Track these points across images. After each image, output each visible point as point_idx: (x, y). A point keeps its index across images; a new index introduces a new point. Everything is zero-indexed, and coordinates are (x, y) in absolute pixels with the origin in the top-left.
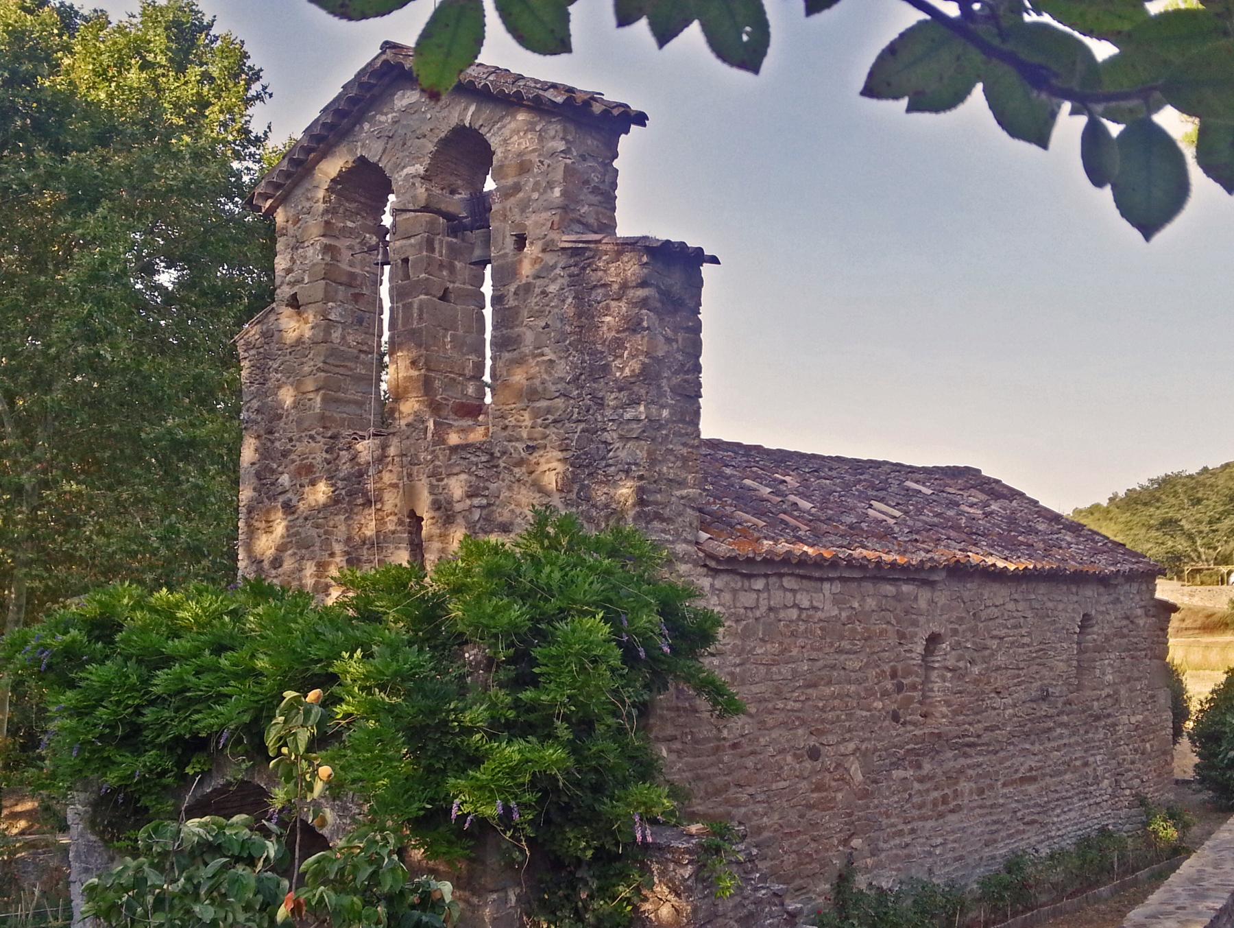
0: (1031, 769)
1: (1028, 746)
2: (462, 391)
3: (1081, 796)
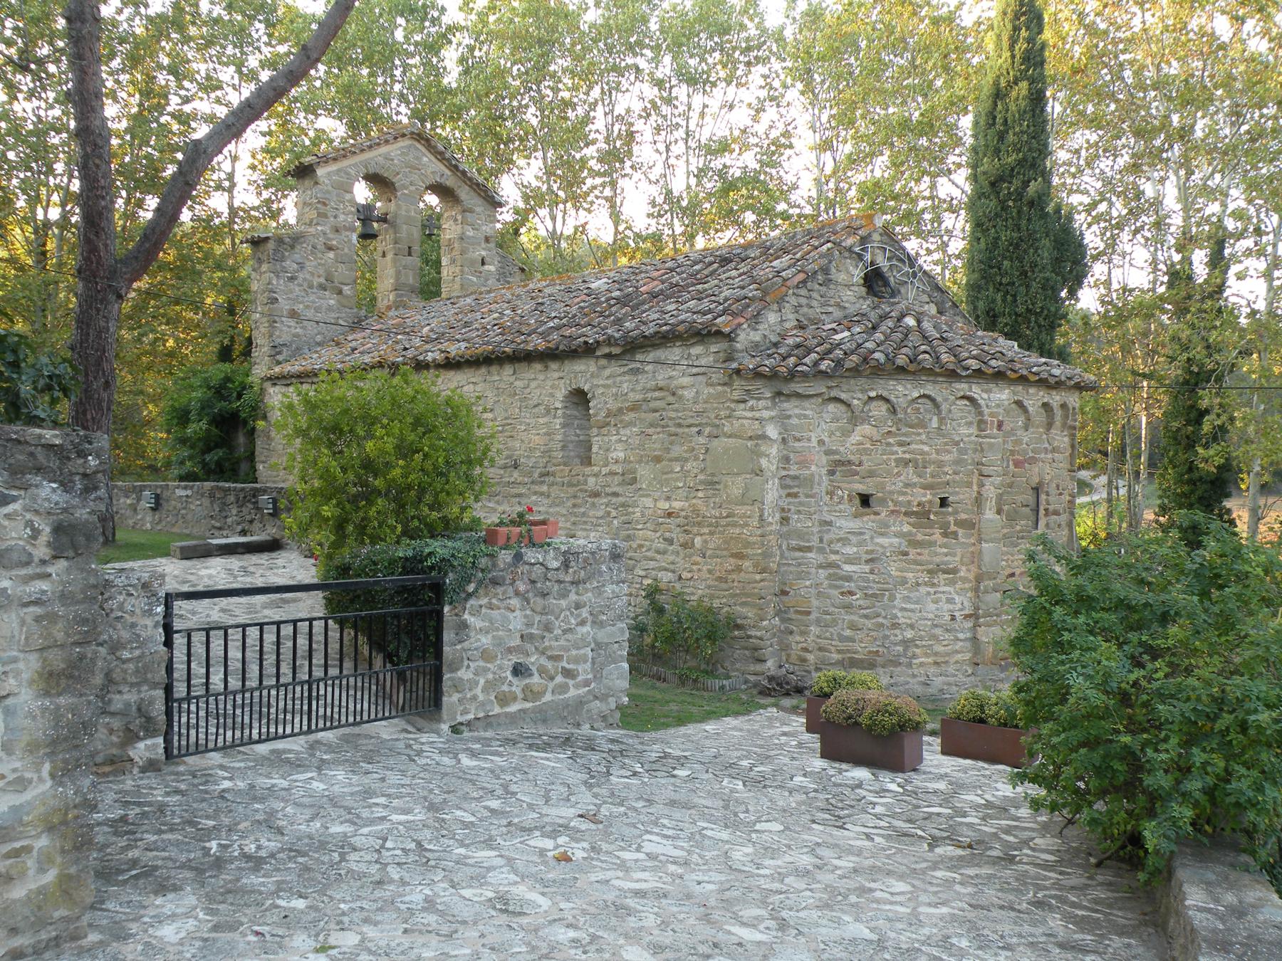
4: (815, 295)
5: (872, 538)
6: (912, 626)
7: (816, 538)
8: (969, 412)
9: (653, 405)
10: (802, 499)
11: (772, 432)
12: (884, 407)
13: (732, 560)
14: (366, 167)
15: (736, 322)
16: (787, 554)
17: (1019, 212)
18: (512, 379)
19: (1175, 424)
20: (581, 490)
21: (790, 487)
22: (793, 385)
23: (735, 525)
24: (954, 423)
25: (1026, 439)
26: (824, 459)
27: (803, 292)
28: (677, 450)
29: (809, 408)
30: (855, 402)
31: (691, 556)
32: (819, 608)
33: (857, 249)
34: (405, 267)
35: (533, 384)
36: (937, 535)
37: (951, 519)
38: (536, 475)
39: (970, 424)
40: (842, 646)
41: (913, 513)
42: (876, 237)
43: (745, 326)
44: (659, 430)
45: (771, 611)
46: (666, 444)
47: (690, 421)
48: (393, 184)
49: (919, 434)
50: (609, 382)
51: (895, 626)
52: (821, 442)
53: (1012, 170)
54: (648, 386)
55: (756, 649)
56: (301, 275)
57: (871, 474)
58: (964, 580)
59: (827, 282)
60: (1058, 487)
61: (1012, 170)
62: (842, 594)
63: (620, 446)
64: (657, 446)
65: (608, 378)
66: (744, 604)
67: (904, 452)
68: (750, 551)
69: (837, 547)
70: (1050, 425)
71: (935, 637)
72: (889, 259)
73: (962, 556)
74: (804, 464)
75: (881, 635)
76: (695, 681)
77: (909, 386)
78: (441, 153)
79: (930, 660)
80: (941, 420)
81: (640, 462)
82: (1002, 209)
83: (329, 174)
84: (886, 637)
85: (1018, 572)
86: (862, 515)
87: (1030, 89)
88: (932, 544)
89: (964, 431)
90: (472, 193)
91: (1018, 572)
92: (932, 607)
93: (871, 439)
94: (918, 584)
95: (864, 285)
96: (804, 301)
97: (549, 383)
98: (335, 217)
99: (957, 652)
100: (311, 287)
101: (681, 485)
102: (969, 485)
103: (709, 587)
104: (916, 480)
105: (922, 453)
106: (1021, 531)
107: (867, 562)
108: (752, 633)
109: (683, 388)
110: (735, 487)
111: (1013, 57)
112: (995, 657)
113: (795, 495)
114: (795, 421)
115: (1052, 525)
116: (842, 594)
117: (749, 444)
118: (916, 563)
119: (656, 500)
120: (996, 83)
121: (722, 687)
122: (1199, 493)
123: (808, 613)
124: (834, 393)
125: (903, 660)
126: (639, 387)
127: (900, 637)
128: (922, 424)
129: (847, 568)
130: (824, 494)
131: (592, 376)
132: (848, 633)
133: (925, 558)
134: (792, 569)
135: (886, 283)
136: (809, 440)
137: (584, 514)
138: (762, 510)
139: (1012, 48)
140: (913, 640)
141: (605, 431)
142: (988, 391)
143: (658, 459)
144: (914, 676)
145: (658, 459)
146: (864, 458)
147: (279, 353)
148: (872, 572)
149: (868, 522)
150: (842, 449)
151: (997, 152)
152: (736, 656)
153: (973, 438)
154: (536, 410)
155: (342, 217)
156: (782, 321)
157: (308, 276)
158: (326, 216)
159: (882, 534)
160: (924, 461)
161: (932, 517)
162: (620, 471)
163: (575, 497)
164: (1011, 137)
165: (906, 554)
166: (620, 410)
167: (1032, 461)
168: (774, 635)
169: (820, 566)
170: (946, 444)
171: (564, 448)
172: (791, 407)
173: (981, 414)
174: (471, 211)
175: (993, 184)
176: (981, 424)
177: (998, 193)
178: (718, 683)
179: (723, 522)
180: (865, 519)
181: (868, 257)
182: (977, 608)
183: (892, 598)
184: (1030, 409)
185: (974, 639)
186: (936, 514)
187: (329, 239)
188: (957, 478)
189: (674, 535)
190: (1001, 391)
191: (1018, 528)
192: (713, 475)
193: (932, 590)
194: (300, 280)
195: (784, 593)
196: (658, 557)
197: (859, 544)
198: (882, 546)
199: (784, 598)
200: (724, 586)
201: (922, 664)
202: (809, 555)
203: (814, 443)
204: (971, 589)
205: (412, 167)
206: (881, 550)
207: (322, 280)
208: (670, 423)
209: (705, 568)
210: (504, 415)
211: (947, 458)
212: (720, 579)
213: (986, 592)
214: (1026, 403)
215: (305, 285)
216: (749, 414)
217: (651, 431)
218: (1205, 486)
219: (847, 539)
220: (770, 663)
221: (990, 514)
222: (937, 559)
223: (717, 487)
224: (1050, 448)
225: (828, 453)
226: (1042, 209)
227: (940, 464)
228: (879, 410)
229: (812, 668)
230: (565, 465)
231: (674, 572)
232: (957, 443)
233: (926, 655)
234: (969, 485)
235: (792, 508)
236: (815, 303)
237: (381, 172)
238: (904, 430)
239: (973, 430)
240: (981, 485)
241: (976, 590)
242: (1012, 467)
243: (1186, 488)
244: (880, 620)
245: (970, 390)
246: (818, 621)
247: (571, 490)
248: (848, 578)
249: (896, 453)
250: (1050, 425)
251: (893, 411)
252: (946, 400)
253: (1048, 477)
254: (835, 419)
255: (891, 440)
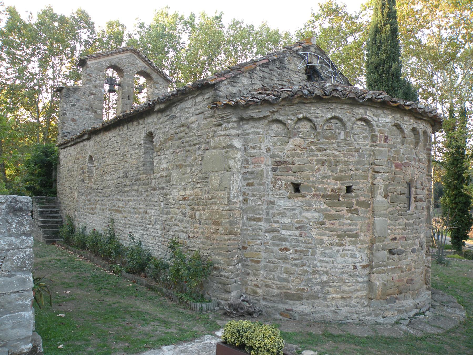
0: (119, 207)
1: (118, 197)
2: (406, 3)
3: (142, 228)
4: (274, 73)
5: (301, 213)
6: (327, 273)
7: (264, 213)
8: (365, 130)
9: (179, 135)
10: (256, 187)
11: (237, 143)
12: (308, 125)
13: (213, 226)
14: (110, 62)
15: (219, 79)
16: (246, 222)
17: (388, 79)
18: (126, 132)
19: (449, 180)
20: (149, 187)
21: (249, 179)
22: (249, 112)
23: (215, 204)
24: (355, 136)
25: (402, 151)
26: (270, 161)
27: (266, 70)
28: (189, 160)
29: (260, 127)
30: (289, 122)
31: (193, 223)
32: (266, 259)
33: (301, 53)
34: (126, 104)
35: (134, 133)
36: (344, 212)
37: (354, 201)
38: (134, 180)
39: (366, 138)
40: (280, 284)
41: (328, 196)
42: (312, 49)
43: (225, 82)
44: (182, 149)
45: (235, 259)
46: (184, 157)
47: (195, 142)
48: (122, 70)
49: (332, 143)
50: (161, 126)
51: (316, 272)
52: (268, 150)
53: (384, 61)
54: (177, 125)
55: (225, 284)
56: (78, 104)
57: (300, 170)
58: (363, 242)
59: (282, 67)
60: (422, 183)
61: (384, 61)
62: (281, 250)
63: (165, 161)
64: (180, 159)
65: (161, 124)
66: (219, 254)
67: (322, 155)
68: (222, 221)
69: (278, 218)
70: (417, 144)
71: (342, 280)
72: (320, 63)
73: (362, 226)
74: (257, 164)
75: (306, 278)
76: (186, 302)
77: (324, 110)
78: (144, 58)
79: (339, 296)
80: (347, 134)
81: (173, 169)
82: (380, 78)
83: (93, 64)
84: (309, 280)
85: (398, 237)
86: (294, 197)
87: (391, 28)
88: (341, 217)
89: (362, 142)
90: (158, 76)
91: (398, 237)
92: (340, 260)
93: (300, 147)
94: (331, 244)
95: (306, 74)
96: (267, 75)
97: (139, 131)
98: (95, 81)
99: (357, 290)
100: (82, 109)
101: (190, 180)
102: (366, 178)
103: (202, 243)
104: (330, 174)
105: (334, 156)
106: (399, 211)
107: (297, 228)
108: (223, 273)
109: (192, 123)
110: (215, 180)
111: (383, 15)
112: (383, 294)
113: (251, 184)
114: (251, 136)
115: (419, 208)
116: (281, 250)
117: (223, 151)
118: (330, 230)
119: (179, 191)
120: (376, 27)
121: (201, 309)
122: (459, 207)
123: (259, 262)
124: (276, 116)
125: (320, 295)
126: (173, 126)
127: (319, 280)
128: (334, 137)
129: (284, 232)
130: (269, 183)
131: (155, 124)
132: (284, 276)
133: (336, 226)
134: (249, 232)
135: (319, 76)
136: (260, 148)
137: (150, 200)
138: (229, 194)
139: (382, 11)
140: (327, 282)
141: (159, 153)
142: (378, 116)
143: (180, 167)
144: (328, 306)
145: (180, 167)
146: (296, 159)
147: (66, 136)
148: (300, 235)
149: (298, 202)
150: (281, 154)
151: (377, 54)
152: (214, 287)
153: (368, 147)
154: (134, 146)
155: (98, 82)
156: (252, 84)
157: (81, 105)
158: (90, 81)
159: (307, 210)
160: (336, 161)
161: (341, 199)
162: (164, 175)
163: (147, 191)
164: (383, 48)
165: (323, 224)
166: (165, 141)
167: (407, 165)
168: (238, 275)
169: (267, 231)
170: (350, 150)
171: (144, 165)
172: (249, 127)
173: (373, 131)
174: (157, 83)
175: (376, 68)
176: (373, 138)
177: (378, 71)
178: (198, 305)
179: (209, 202)
180: (296, 200)
181: (308, 58)
182: (371, 261)
183: (314, 253)
184: (405, 130)
185: (369, 282)
186: (343, 197)
187: (92, 90)
188: (358, 173)
189: (187, 211)
190: (387, 115)
191: (398, 208)
192: (205, 173)
193: (341, 249)
194: (77, 106)
195: (245, 248)
196: (179, 224)
197: (292, 217)
198: (307, 218)
199: (244, 251)
200: (209, 242)
201: (333, 299)
202: (260, 223)
203: (263, 150)
204: (367, 248)
205: (131, 64)
206: (306, 221)
207: (88, 107)
208: (186, 145)
209: (200, 231)
210: (123, 151)
211: (351, 159)
212: (207, 238)
213: (377, 250)
214: (402, 126)
215: (79, 109)
216: (223, 133)
217: (177, 151)
218: (461, 205)
219: (284, 213)
220: (234, 294)
221: (380, 198)
222: (345, 228)
223: (207, 180)
224: (417, 158)
225: (272, 156)
226: (398, 78)
227: (346, 164)
228: (305, 127)
229: (261, 298)
230: (144, 174)
231: (186, 233)
232: (357, 150)
233: (336, 292)
234: (366, 178)
235: (250, 193)
236: (274, 78)
237: (117, 65)
238: (322, 140)
239: (368, 142)
240: (374, 178)
241: (371, 249)
242: (394, 168)
243: (454, 206)
244: (306, 268)
245: (366, 114)
246: (265, 267)
247: (146, 187)
248: (285, 240)
249: (317, 156)
250: (417, 144)
251: (314, 128)
252: (350, 120)
253: (416, 177)
254: (277, 135)
255: (313, 147)
